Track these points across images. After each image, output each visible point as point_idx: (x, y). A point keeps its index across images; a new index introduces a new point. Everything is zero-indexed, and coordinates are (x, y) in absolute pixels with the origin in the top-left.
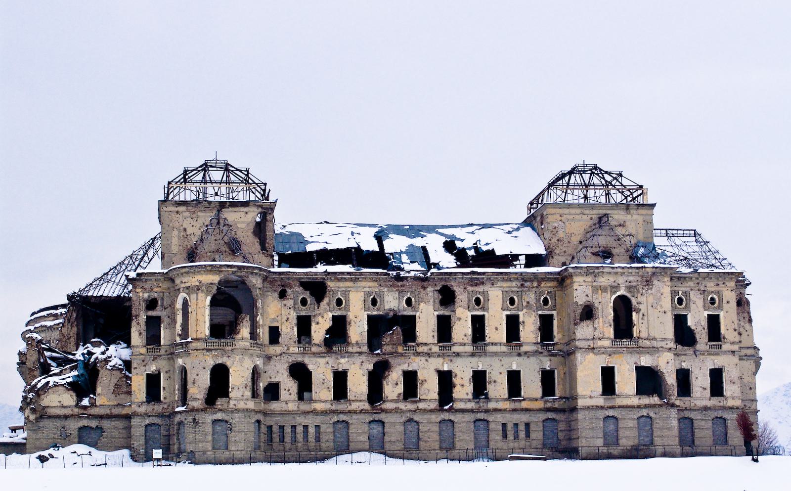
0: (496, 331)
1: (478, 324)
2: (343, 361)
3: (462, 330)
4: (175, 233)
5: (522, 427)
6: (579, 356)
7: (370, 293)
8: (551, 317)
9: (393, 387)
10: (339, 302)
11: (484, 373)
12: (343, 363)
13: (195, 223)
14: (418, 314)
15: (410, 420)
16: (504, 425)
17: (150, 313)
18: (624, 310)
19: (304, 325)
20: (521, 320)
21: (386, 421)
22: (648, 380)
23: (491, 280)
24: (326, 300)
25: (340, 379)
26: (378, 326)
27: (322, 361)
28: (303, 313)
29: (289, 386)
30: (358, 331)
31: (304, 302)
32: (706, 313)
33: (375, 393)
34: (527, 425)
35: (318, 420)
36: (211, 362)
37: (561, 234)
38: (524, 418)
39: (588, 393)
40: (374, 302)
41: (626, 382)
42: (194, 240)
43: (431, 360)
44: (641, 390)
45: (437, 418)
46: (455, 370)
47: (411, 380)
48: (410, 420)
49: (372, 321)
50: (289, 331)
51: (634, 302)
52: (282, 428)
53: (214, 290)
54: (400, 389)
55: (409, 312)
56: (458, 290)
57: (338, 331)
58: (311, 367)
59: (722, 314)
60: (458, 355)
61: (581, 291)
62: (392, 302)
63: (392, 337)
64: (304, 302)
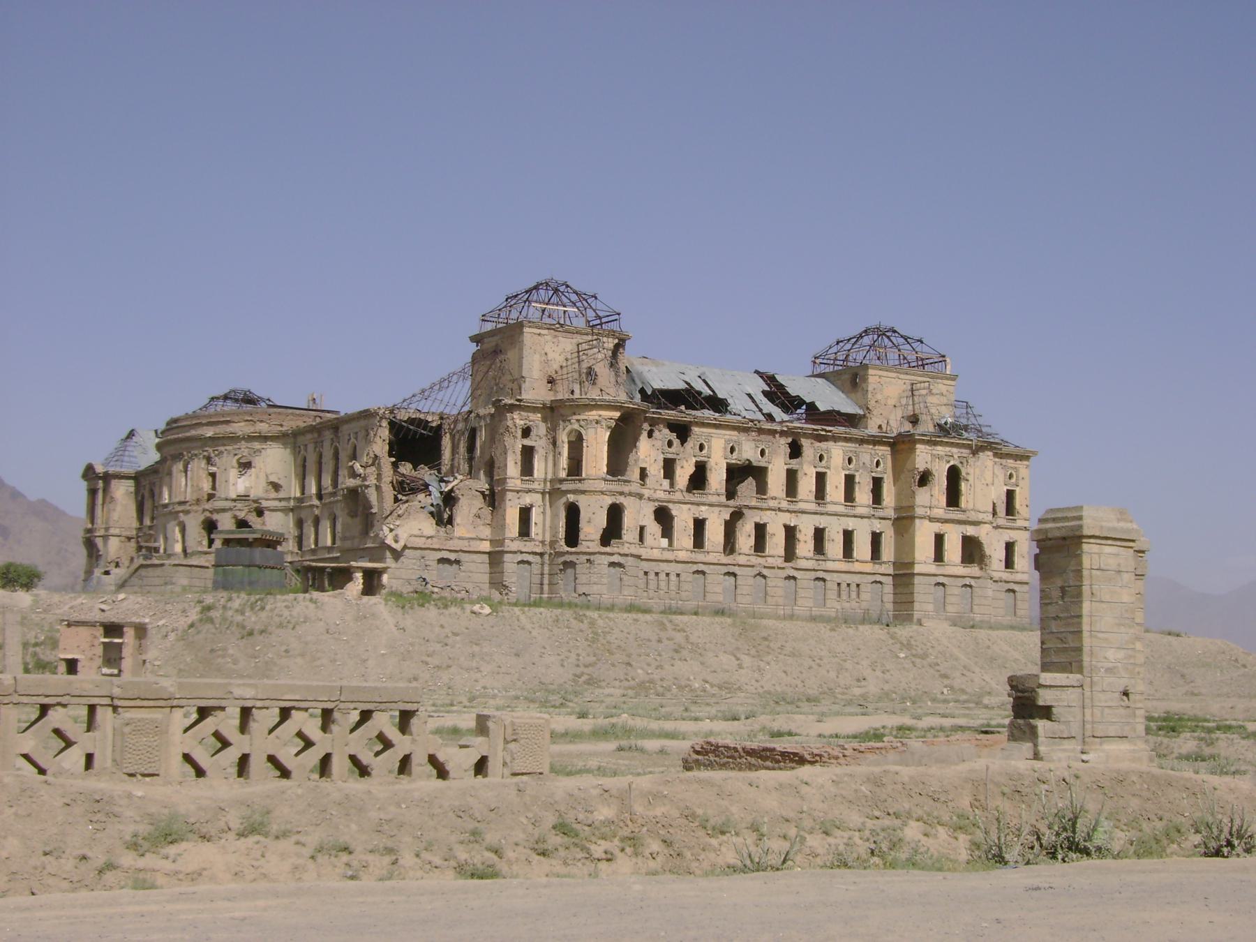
0: (835, 490)
1: (821, 478)
3: (807, 485)
4: (537, 357)
5: (853, 587)
6: (917, 521)
9: (745, 539)
10: (701, 447)
11: (794, 528)
12: (703, 512)
13: (555, 348)
15: (760, 574)
17: (527, 442)
18: (954, 476)
19: (669, 468)
20: (857, 480)
22: (972, 550)
23: (835, 439)
25: (699, 525)
26: (738, 473)
28: (670, 456)
29: (654, 528)
30: (717, 478)
31: (670, 444)
32: (1005, 488)
33: (730, 544)
36: (609, 500)
37: (879, 397)
39: (924, 559)
40: (732, 450)
41: (953, 550)
42: (556, 366)
46: (801, 527)
47: (760, 530)
48: (760, 574)
50: (656, 470)
53: (613, 424)
54: (752, 541)
55: (762, 464)
57: (698, 480)
58: (674, 513)
59: (1018, 490)
61: (923, 457)
62: (748, 451)
63: (747, 487)
64: (670, 444)
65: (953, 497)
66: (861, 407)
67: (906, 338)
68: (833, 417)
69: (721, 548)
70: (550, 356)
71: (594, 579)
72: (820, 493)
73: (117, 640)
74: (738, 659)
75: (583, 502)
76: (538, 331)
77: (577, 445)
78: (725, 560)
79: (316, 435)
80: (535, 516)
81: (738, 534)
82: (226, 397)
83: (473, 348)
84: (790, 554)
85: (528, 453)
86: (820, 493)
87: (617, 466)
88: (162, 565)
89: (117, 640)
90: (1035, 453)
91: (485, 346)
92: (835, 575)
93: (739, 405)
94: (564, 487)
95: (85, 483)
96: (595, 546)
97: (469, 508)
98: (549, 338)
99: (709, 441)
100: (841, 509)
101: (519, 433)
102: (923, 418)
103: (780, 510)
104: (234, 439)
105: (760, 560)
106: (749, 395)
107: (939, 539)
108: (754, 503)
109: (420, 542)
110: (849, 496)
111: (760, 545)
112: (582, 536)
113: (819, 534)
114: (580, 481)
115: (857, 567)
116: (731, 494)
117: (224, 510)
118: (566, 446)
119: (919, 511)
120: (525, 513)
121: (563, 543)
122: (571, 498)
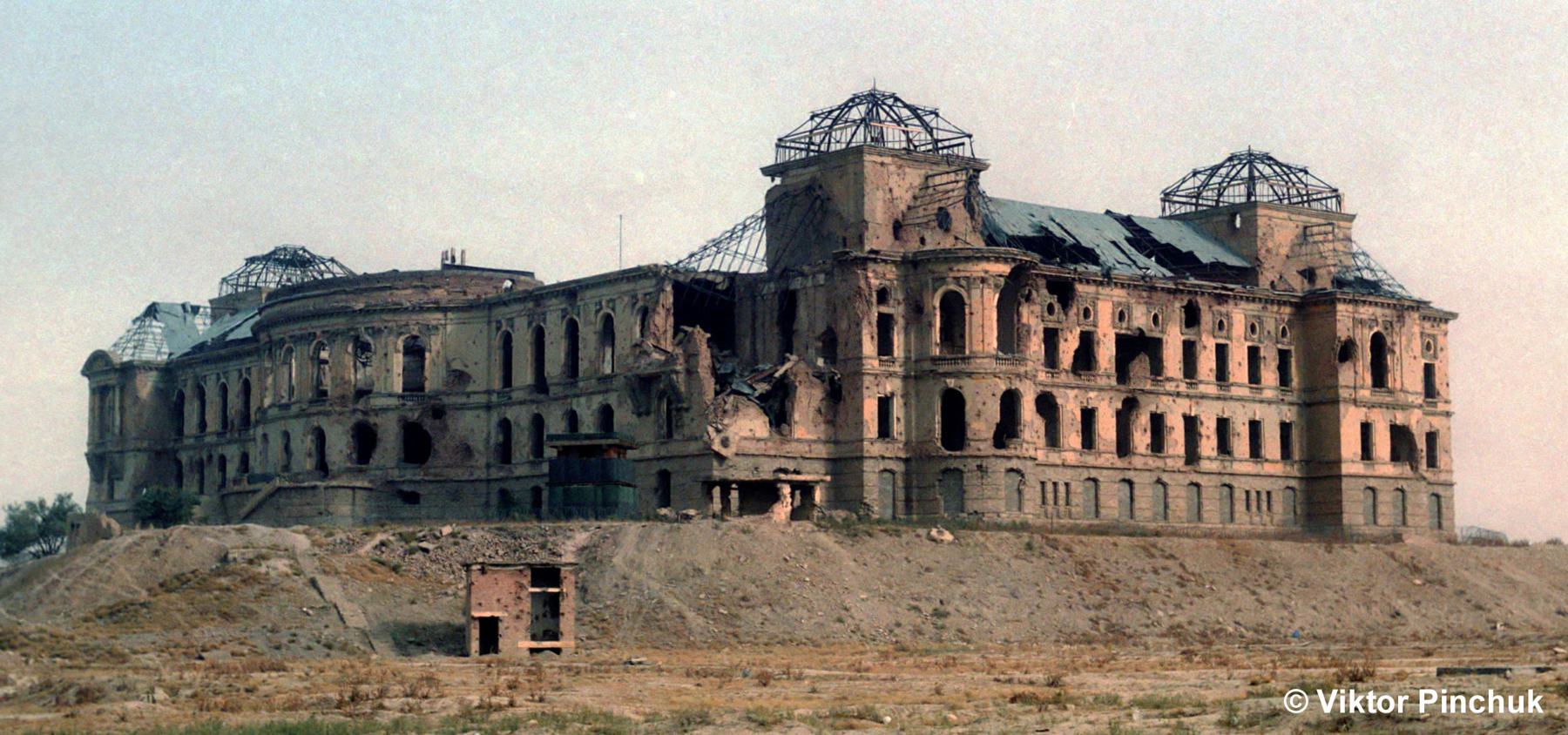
1: (1221, 351)
2: (1092, 394)
3: (1207, 362)
7: (1120, 304)
8: (1288, 351)
9: (1141, 439)
10: (1086, 313)
12: (1260, 412)
14: (1165, 338)
15: (1159, 481)
16: (1247, 492)
17: (885, 309)
21: (1135, 480)
24: (1074, 310)
25: (1088, 416)
27: (1071, 393)
28: (1051, 325)
30: (1106, 353)
31: (1051, 309)
33: (1124, 446)
34: (1269, 493)
35: (1068, 475)
36: (1003, 386)
37: (1270, 245)
38: (1264, 485)
40: (1121, 316)
41: (1382, 444)
43: (1179, 400)
44: (1395, 457)
45: (1184, 480)
47: (1157, 421)
49: (1121, 341)
51: (1389, 341)
52: (1055, 484)
54: (1147, 439)
55: (1156, 335)
56: (1204, 307)
57: (1085, 358)
58: (1059, 401)
60: (1203, 397)
62: (1140, 319)
63: (1140, 366)
64: (1051, 309)
65: (1379, 375)
66: (1244, 258)
67: (913, 110)
68: (1216, 271)
69: (1114, 448)
70: (896, 193)
71: (988, 493)
72: (1222, 374)
73: (551, 590)
74: (1254, 593)
75: (968, 388)
76: (879, 159)
77: (954, 309)
78: (1119, 463)
79: (531, 305)
80: (897, 409)
81: (1133, 428)
82: (267, 258)
83: (767, 183)
84: (1192, 456)
85: (885, 323)
86: (1222, 374)
87: (1010, 337)
88: (314, 488)
89: (551, 590)
90: (1454, 316)
91: (788, 181)
92: (1243, 479)
93: (1109, 256)
94: (942, 369)
95: (86, 381)
96: (987, 448)
97: (807, 401)
98: (892, 168)
99: (1095, 305)
100: (1245, 392)
101: (874, 299)
102: (1320, 272)
103: (1178, 394)
104: (398, 309)
105: (1159, 463)
106: (1114, 243)
107: (1366, 429)
108: (1148, 387)
109: (751, 447)
110: (1254, 377)
111: (1157, 445)
112: (969, 435)
113: (1223, 425)
114: (963, 359)
115: (1268, 468)
116: (1122, 372)
117: (385, 410)
118: (938, 313)
119: (1344, 393)
120: (885, 404)
121: (939, 444)
122: (951, 383)
